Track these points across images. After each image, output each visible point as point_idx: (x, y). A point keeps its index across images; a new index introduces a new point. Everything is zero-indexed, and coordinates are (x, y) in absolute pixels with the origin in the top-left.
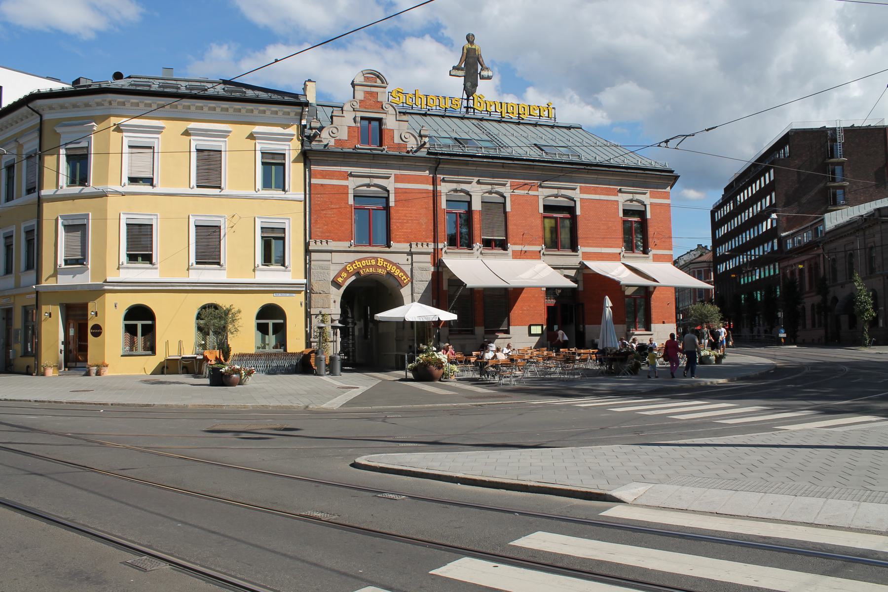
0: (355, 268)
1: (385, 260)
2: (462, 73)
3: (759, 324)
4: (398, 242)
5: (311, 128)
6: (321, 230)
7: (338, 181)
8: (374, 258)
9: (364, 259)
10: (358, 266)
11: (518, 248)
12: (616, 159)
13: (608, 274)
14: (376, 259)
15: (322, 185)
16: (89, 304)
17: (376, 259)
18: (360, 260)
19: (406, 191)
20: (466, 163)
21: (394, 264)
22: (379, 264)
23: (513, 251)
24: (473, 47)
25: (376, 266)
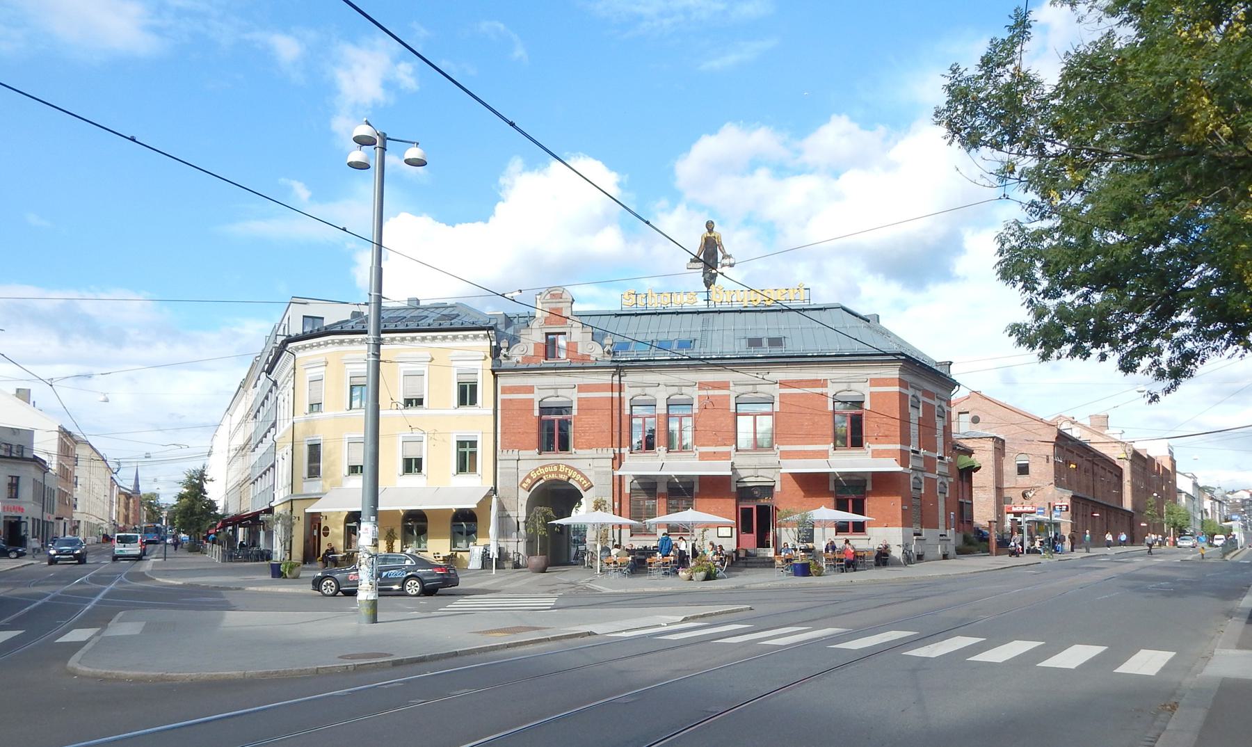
0: (539, 474)
1: (567, 466)
2: (701, 265)
3: (289, 529)
4: (581, 449)
5: (1228, 210)
6: (509, 440)
7: (905, 340)
8: (556, 465)
9: (547, 466)
10: (541, 473)
11: (874, 447)
12: (859, 325)
13: (1061, 491)
14: (558, 465)
15: (510, 400)
16: (866, 501)
17: (558, 465)
18: (543, 467)
19: (587, 399)
20: (650, 367)
21: (575, 470)
22: (560, 470)
23: (873, 451)
24: (713, 235)
25: (558, 473)
